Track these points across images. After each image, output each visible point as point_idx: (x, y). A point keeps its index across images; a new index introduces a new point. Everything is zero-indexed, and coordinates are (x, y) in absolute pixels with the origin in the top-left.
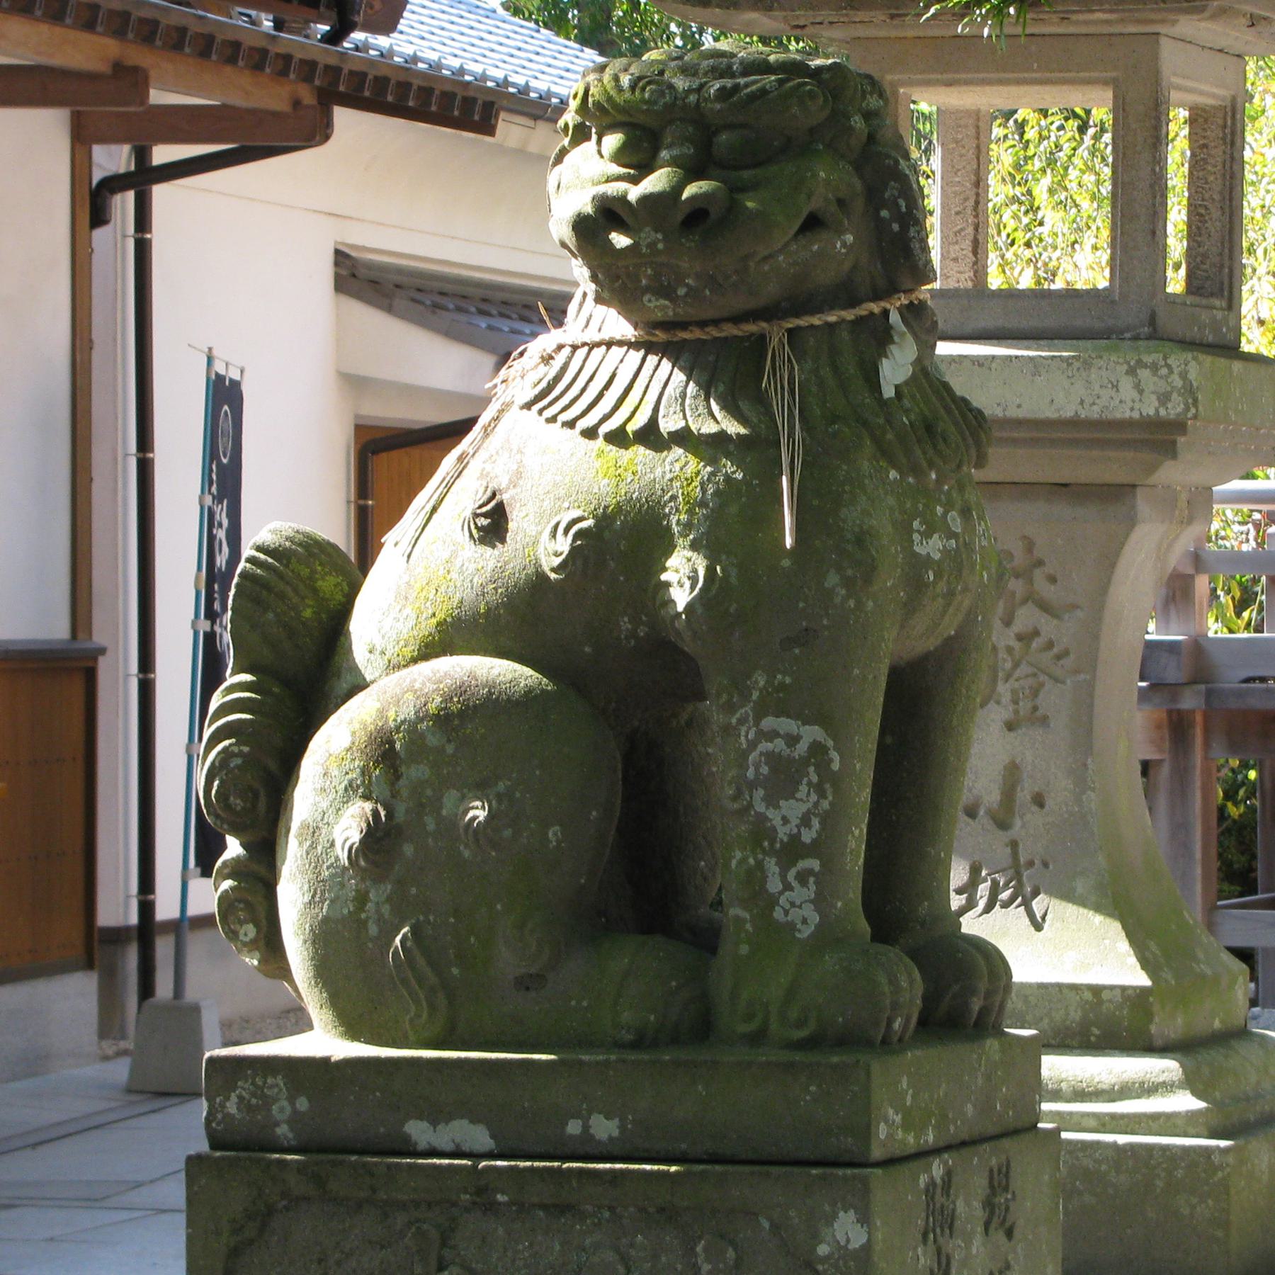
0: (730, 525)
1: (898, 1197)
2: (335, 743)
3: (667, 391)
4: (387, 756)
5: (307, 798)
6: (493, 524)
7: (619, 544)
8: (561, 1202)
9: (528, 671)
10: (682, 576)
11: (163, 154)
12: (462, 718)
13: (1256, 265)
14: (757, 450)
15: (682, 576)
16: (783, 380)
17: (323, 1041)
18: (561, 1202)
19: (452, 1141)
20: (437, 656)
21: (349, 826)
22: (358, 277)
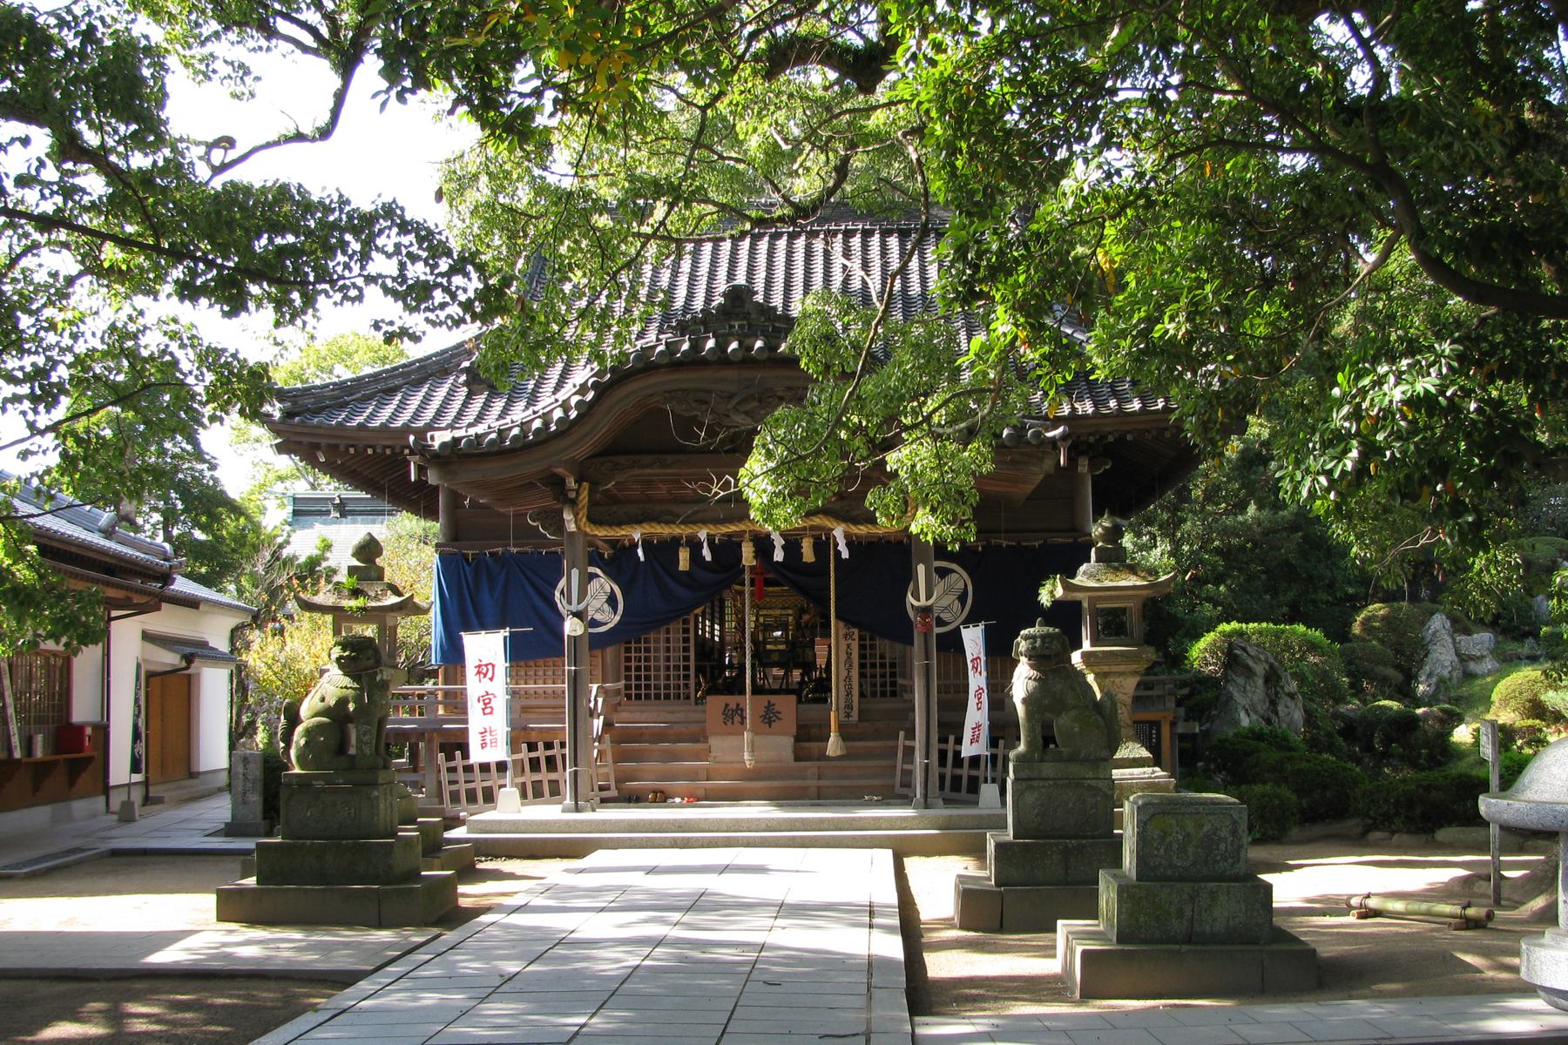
0: (358, 700)
1: (381, 789)
2: (300, 729)
3: (347, 681)
4: (308, 732)
5: (295, 738)
6: (323, 700)
7: (342, 702)
8: (335, 791)
9: (1102, 886)
10: (351, 707)
11: (114, 613)
12: (319, 726)
13: (325, 655)
14: (361, 689)
15: (351, 707)
16: (364, 679)
17: (297, 770)
18: (335, 791)
19: (319, 784)
20: (941, 853)
21: (302, 742)
22: (147, 637)
